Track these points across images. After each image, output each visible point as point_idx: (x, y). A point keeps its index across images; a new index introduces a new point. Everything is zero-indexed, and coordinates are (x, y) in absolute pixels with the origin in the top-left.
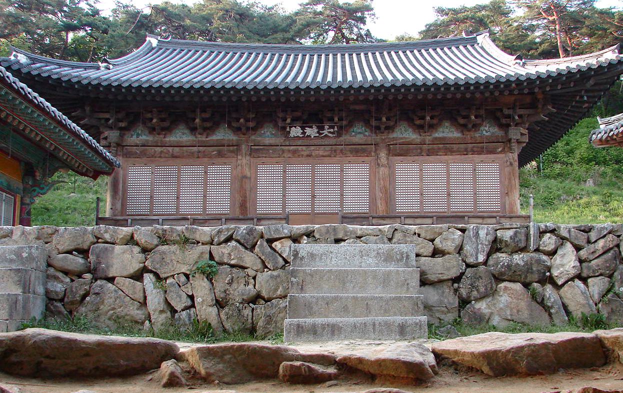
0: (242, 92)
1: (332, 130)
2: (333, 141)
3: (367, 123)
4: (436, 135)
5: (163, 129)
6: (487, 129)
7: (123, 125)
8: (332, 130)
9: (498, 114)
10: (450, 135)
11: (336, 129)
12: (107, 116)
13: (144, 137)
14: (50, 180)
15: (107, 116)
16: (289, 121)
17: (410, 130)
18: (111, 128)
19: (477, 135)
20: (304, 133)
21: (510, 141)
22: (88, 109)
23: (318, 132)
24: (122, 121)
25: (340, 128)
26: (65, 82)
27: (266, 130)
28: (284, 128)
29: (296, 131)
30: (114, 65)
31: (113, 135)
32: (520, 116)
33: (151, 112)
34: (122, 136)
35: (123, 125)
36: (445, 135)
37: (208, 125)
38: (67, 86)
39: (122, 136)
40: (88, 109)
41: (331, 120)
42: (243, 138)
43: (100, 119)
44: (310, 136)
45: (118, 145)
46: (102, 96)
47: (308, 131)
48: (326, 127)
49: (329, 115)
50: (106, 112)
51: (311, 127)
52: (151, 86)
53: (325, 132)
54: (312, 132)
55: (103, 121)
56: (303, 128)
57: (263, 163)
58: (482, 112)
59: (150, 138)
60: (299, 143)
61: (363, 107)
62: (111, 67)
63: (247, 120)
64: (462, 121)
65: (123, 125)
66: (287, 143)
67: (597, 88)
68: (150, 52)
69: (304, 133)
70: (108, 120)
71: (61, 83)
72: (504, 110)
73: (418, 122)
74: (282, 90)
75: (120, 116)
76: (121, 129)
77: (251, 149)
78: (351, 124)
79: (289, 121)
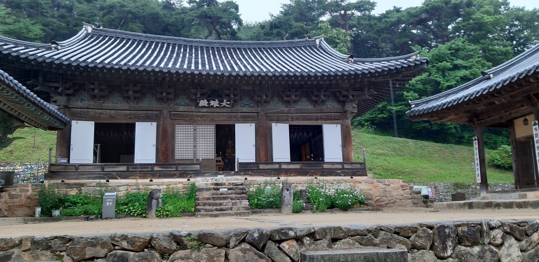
0: (159, 74)
1: (229, 103)
2: (229, 110)
3: (252, 98)
4: (297, 107)
5: (102, 97)
6: (330, 103)
7: (70, 93)
8: (229, 103)
9: (338, 94)
10: (306, 107)
11: (232, 102)
12: (56, 85)
13: (87, 102)
14: (9, 136)
15: (56, 85)
16: (199, 96)
17: (280, 103)
18: (60, 94)
19: (324, 108)
20: (209, 104)
21: (346, 112)
22: (41, 79)
23: (219, 104)
24: (69, 89)
25: (235, 101)
26: (23, 59)
27: (181, 101)
28: (196, 100)
29: (203, 103)
30: (61, 46)
31: (62, 100)
32: (353, 96)
33: (93, 84)
34: (68, 100)
35: (70, 92)
36: (303, 107)
37: (138, 95)
38: (24, 62)
39: (68, 100)
40: (41, 79)
41: (228, 95)
42: (165, 105)
43: (51, 87)
44: (213, 106)
45: (66, 107)
46: (53, 71)
47: (212, 103)
48: (225, 101)
49: (227, 92)
50: (57, 82)
51: (214, 100)
52: (95, 66)
53: (224, 104)
54: (215, 103)
55: (53, 89)
56: (208, 101)
57: (179, 124)
58: (328, 93)
59: (92, 103)
60: (205, 110)
61: (250, 88)
62: (59, 47)
63: (168, 94)
64: (314, 99)
65: (70, 92)
66: (197, 110)
67: (404, 79)
68: (83, 39)
69: (209, 104)
70: (58, 88)
71: (62, 66)
72: (342, 92)
73: (286, 99)
74: (197, 75)
75: (67, 85)
76: (68, 95)
77: (171, 114)
78: (176, 96)
79: (199, 96)
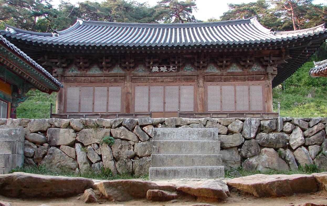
0: (127, 48)
1: (174, 68)
2: (175, 74)
3: (193, 64)
4: (229, 71)
5: (86, 68)
6: (255, 67)
7: (65, 66)
8: (174, 68)
9: (262, 60)
10: (236, 71)
11: (176, 68)
12: (56, 61)
13: (76, 72)
14: (26, 94)
15: (56, 61)
16: (151, 63)
17: (215, 68)
18: (58, 67)
19: (250, 71)
20: (159, 70)
21: (267, 74)
22: (46, 57)
23: (167, 69)
24: (64, 64)
25: (179, 67)
26: (34, 43)
27: (139, 68)
28: (149, 67)
29: (155, 69)
30: (60, 34)
31: (59, 71)
32: (273, 61)
33: (79, 59)
34: (64, 71)
35: (64, 65)
36: (233, 71)
37: (109, 65)
38: (35, 45)
39: (64, 71)
40: (46, 57)
41: (174, 63)
42: (128, 72)
43: (52, 62)
44: (162, 71)
45: (62, 76)
46: (53, 50)
47: (162, 69)
48: (171, 67)
49: (173, 60)
50: (56, 59)
51: (163, 67)
52: (79, 45)
53: (171, 69)
54: (164, 69)
55: (54, 64)
56: (159, 67)
57: (138, 86)
58: (253, 59)
59: (79, 72)
60: (157, 75)
61: (190, 56)
62: (58, 35)
63: (130, 63)
64: (242, 64)
65: (64, 65)
66: (151, 75)
67: (313, 46)
68: (79, 27)
69: (159, 70)
70: (56, 63)
71: (32, 44)
72: (265, 58)
73: (219, 64)
74: (148, 47)
75: (63, 61)
76: (63, 68)
77: (132, 78)
78: (184, 65)
79: (151, 63)
